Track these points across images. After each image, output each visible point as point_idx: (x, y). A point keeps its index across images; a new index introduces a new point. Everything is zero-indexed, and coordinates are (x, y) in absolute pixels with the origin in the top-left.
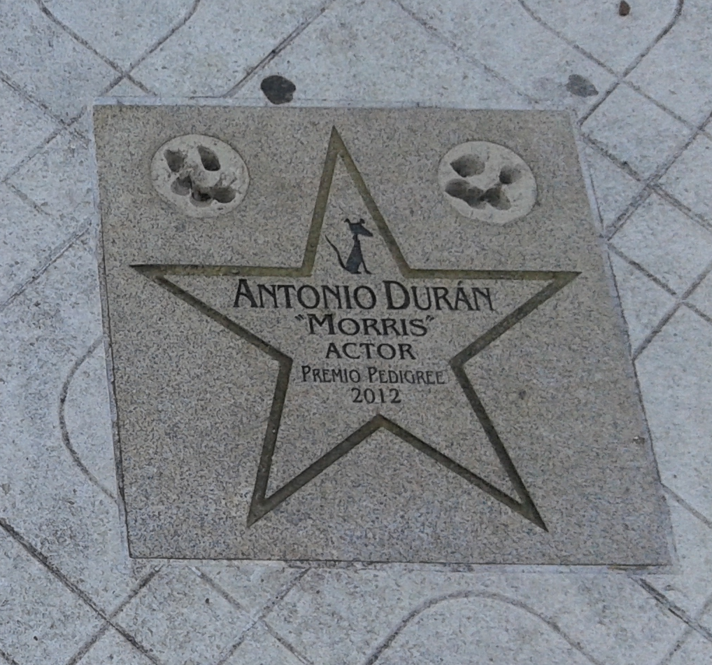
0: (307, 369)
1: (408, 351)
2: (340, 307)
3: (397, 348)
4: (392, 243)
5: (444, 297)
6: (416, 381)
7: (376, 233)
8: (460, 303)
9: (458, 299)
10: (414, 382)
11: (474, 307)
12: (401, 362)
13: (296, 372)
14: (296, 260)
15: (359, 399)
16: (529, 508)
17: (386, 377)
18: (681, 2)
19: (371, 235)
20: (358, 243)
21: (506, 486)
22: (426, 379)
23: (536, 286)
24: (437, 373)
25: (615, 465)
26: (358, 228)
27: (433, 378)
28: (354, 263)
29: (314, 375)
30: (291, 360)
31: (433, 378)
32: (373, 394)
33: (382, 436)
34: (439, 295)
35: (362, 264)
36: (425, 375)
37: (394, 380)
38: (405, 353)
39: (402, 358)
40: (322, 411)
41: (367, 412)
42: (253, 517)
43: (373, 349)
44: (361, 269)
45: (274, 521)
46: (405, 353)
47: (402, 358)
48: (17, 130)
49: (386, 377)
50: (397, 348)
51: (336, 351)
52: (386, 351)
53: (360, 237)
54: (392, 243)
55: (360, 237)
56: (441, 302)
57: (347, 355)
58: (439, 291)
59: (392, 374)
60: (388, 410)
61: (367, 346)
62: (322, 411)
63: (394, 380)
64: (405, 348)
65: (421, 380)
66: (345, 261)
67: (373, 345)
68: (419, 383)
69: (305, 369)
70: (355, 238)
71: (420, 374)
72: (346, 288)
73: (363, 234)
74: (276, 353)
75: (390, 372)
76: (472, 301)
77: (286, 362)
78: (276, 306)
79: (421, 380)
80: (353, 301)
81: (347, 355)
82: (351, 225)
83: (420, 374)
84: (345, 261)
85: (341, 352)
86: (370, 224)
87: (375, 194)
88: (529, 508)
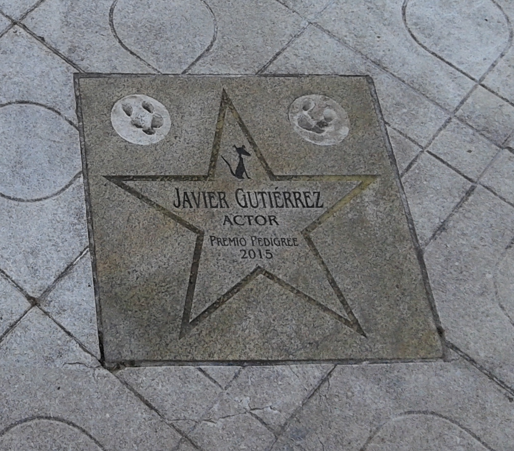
0: (213, 238)
1: (274, 220)
3: (267, 218)
9: (184, 201)
10: (279, 245)
11: (305, 205)
13: (206, 242)
20: (241, 159)
25: (497, 248)
26: (241, 151)
29: (218, 242)
36: (286, 241)
38: (272, 221)
44: (244, 175)
50: (267, 218)
51: (229, 221)
53: (243, 156)
55: (243, 156)
56: (288, 202)
57: (236, 223)
59: (266, 241)
61: (249, 217)
66: (235, 173)
67: (252, 216)
68: (283, 245)
70: (240, 157)
74: (193, 229)
82: (237, 149)
84: (235, 173)
86: (248, 148)
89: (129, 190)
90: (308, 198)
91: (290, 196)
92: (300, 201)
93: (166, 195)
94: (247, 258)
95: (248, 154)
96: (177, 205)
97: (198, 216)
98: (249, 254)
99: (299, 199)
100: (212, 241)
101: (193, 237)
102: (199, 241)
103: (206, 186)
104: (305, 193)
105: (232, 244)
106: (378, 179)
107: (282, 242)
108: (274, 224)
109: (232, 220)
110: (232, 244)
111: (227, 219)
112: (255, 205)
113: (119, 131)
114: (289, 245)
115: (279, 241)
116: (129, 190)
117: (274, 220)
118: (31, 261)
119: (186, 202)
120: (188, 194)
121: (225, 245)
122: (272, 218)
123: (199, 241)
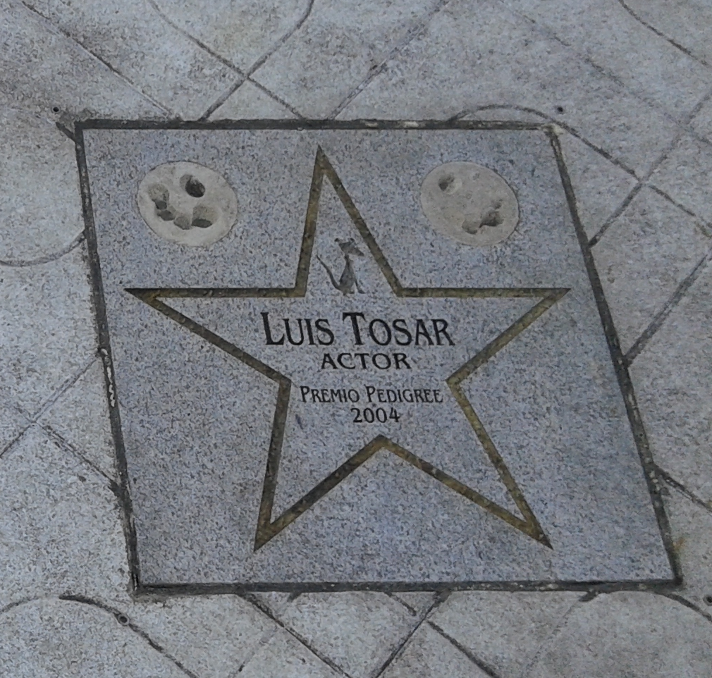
4: (382, 261)
5: (443, 330)
6: (415, 399)
9: (418, 333)
10: (412, 401)
12: (398, 372)
13: (295, 393)
14: (287, 278)
15: (359, 419)
17: (385, 397)
21: (513, 507)
24: (435, 391)
27: (431, 397)
28: (345, 283)
29: (314, 396)
31: (431, 397)
34: (439, 329)
36: (423, 394)
37: (392, 399)
39: (398, 367)
41: (373, 430)
42: (259, 543)
43: (368, 359)
47: (398, 367)
48: (425, 573)
49: (385, 397)
51: (331, 362)
52: (381, 361)
54: (382, 261)
55: (351, 256)
56: (441, 334)
58: (438, 324)
63: (392, 399)
64: (400, 357)
69: (304, 390)
70: (346, 258)
75: (388, 391)
78: (265, 315)
87: (480, 491)
89: (170, 312)
92: (319, 397)
93: (235, 320)
94: (361, 421)
95: (361, 254)
96: (320, 323)
99: (317, 395)
101: (464, 384)
102: (284, 393)
103: (296, 309)
104: (322, 391)
106: (119, 58)
107: (416, 396)
108: (445, 341)
109: (335, 361)
110: (337, 399)
111: (327, 359)
114: (427, 401)
115: (411, 395)
116: (170, 312)
121: (324, 401)
122: (400, 357)
123: (284, 393)
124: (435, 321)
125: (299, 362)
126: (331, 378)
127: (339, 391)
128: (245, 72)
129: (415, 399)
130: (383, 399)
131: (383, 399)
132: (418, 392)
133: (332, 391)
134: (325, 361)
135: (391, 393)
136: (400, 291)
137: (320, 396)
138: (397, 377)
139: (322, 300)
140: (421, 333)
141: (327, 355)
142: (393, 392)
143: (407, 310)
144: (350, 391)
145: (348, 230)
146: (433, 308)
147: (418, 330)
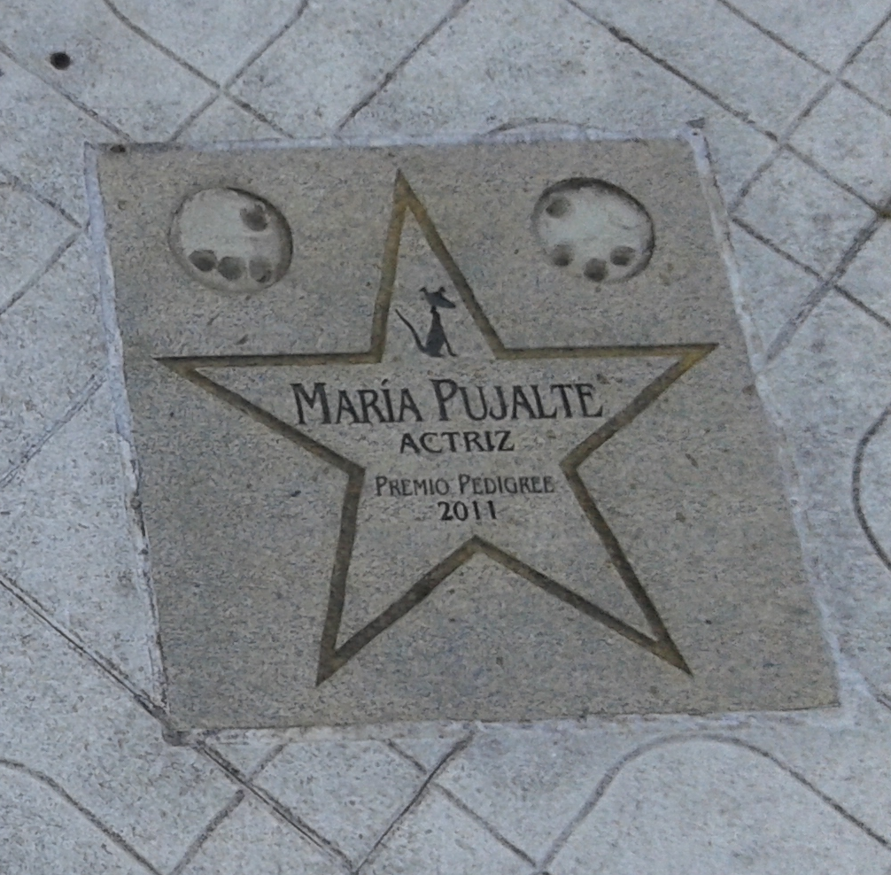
0: (382, 481)
1: (474, 440)
2: (535, 388)
5: (373, 404)
7: (462, 306)
8: (408, 413)
9: (403, 406)
16: (666, 646)
18: (6, 762)
19: (452, 306)
22: (531, 487)
23: (661, 364)
26: (437, 299)
27: (541, 486)
28: (436, 342)
30: (362, 471)
31: (541, 486)
32: (466, 509)
33: (479, 560)
35: (445, 346)
36: (530, 483)
38: (472, 444)
40: (403, 535)
41: (459, 531)
42: (325, 673)
45: (354, 672)
46: (472, 444)
47: (469, 449)
49: (482, 487)
55: (440, 310)
60: (492, 531)
62: (403, 535)
64: (471, 437)
65: (525, 489)
66: (424, 343)
68: (522, 491)
69: (381, 481)
70: (433, 311)
71: (369, 397)
72: (431, 481)
73: (443, 306)
76: (359, 412)
77: (355, 472)
79: (525, 489)
80: (435, 489)
81: (427, 449)
83: (369, 397)
85: (419, 446)
86: (453, 296)
88: (666, 646)
90: (586, 398)
91: (376, 396)
95: (452, 306)
97: (345, 437)
98: (455, 512)
99: (373, 404)
100: (379, 486)
101: (337, 483)
103: (373, 375)
105: (420, 492)
107: (522, 485)
110: (420, 492)
112: (479, 415)
113: (103, 280)
115: (515, 485)
117: (474, 440)
118: (796, 797)
119: (344, 413)
120: (524, 391)
122: (471, 437)
124: (362, 393)
125: (375, 446)
126: (410, 465)
127: (424, 482)
128: (222, 82)
129: (519, 488)
130: (478, 490)
131: (478, 490)
132: (394, 484)
133: (415, 482)
134: (404, 443)
135: (489, 482)
136: (500, 349)
137: (399, 489)
138: (483, 464)
139: (407, 369)
140: (520, 404)
141: (407, 436)
142: (493, 481)
143: (516, 374)
144: (438, 481)
145: (434, 275)
146: (570, 370)
147: (341, 403)
